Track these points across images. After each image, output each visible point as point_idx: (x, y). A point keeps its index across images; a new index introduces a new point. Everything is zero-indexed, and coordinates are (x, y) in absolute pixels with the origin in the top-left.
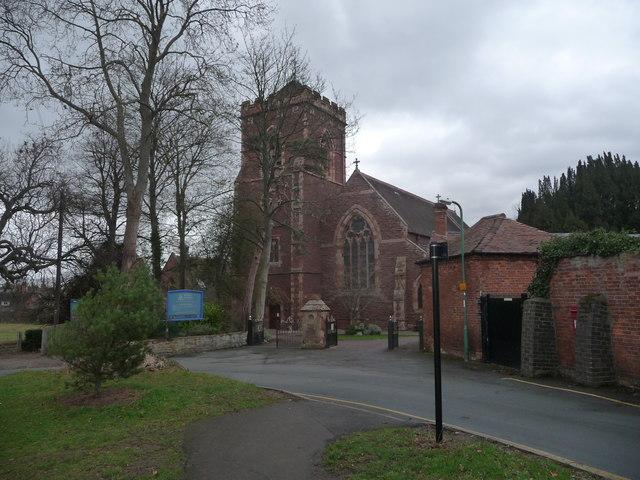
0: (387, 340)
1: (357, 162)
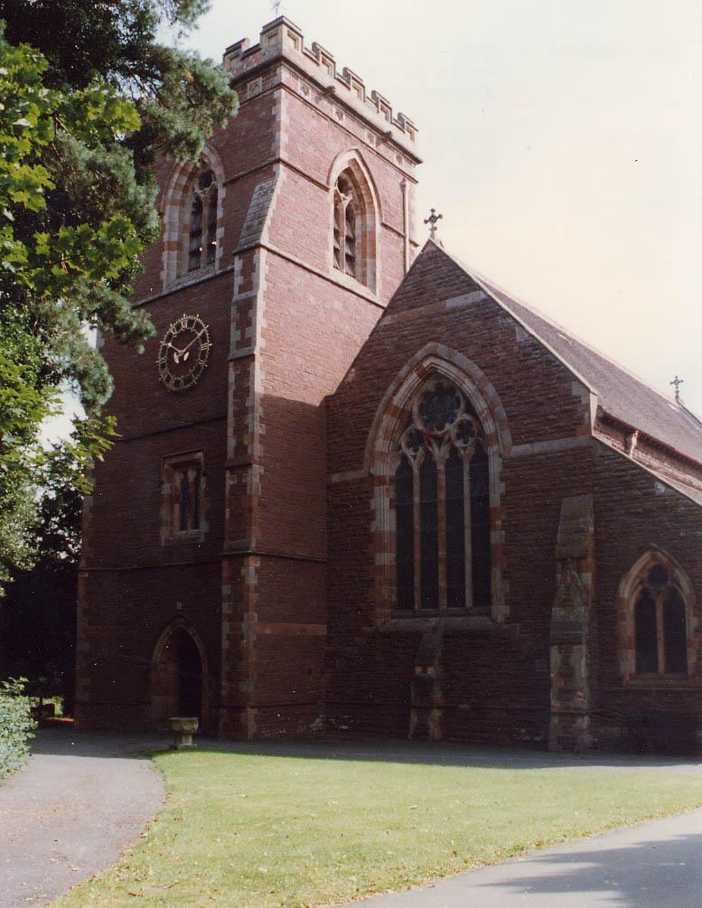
0: (256, 390)
1: (433, 219)
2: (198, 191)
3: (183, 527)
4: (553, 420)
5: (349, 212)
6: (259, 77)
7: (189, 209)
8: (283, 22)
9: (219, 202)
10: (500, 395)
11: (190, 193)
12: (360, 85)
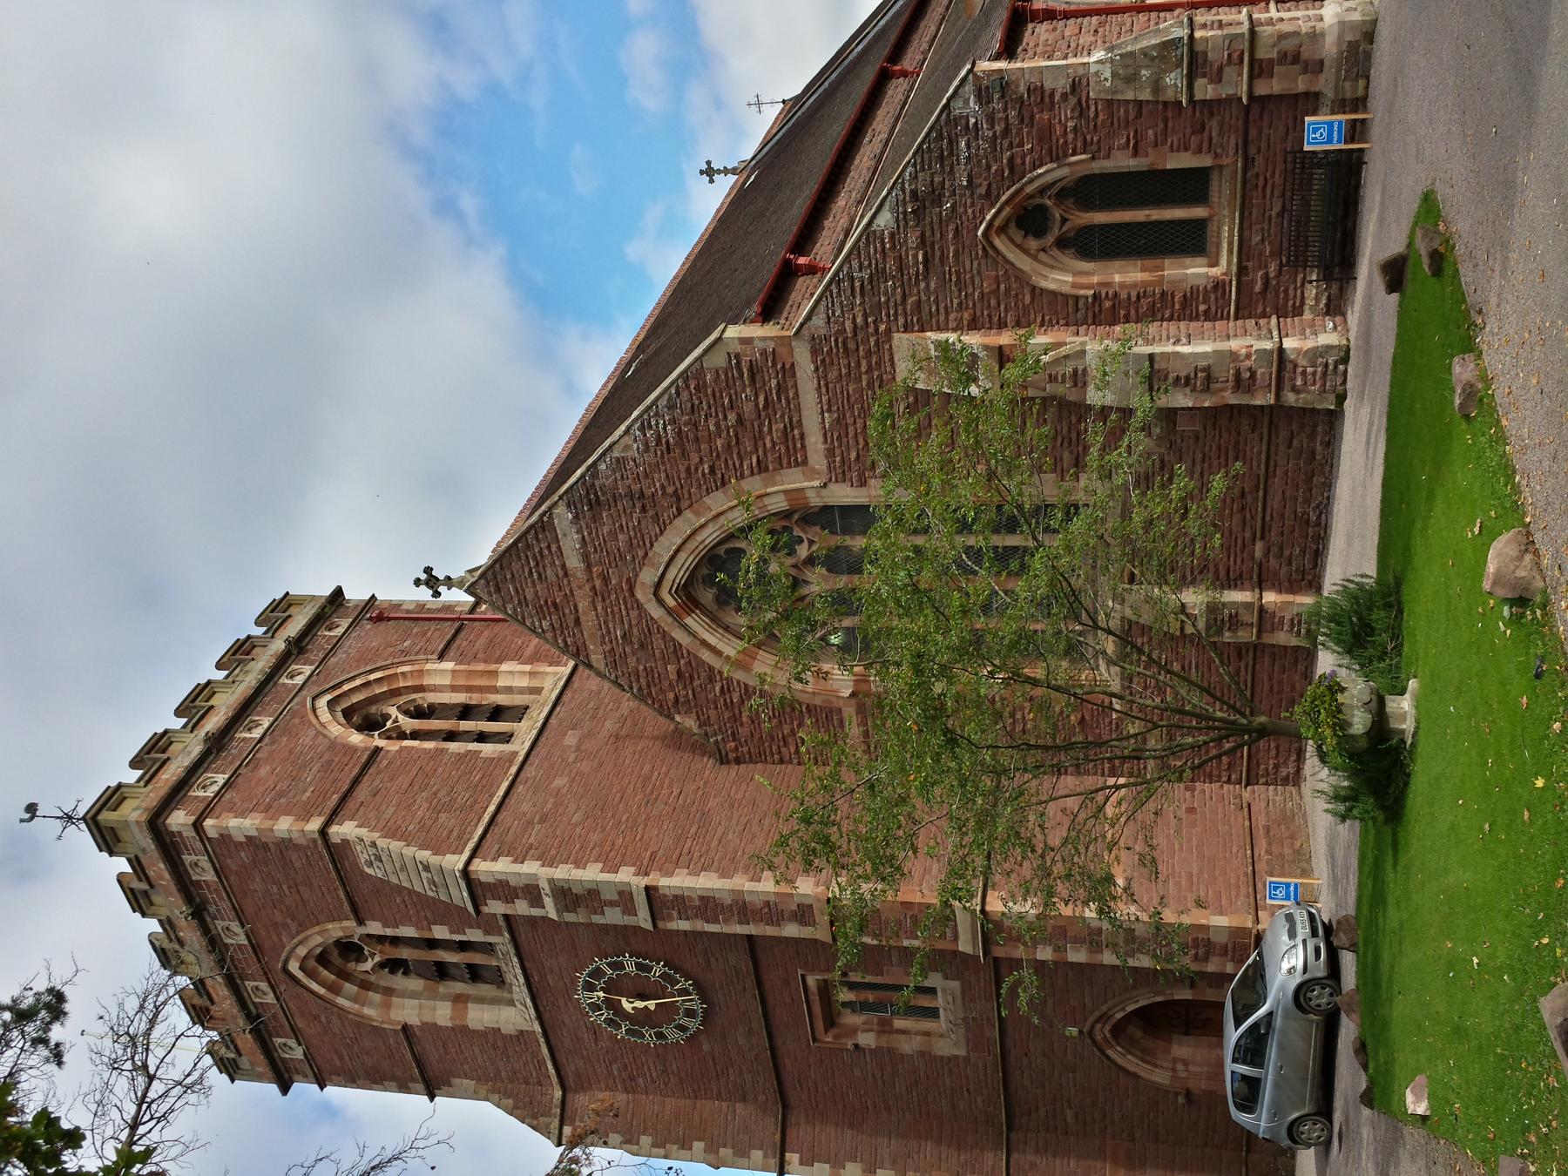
2: (368, 965)
3: (933, 1013)
4: (766, 399)
5: (419, 713)
6: (181, 859)
7: (399, 981)
8: (94, 818)
9: (389, 932)
10: (724, 484)
11: (373, 978)
12: (204, 691)
